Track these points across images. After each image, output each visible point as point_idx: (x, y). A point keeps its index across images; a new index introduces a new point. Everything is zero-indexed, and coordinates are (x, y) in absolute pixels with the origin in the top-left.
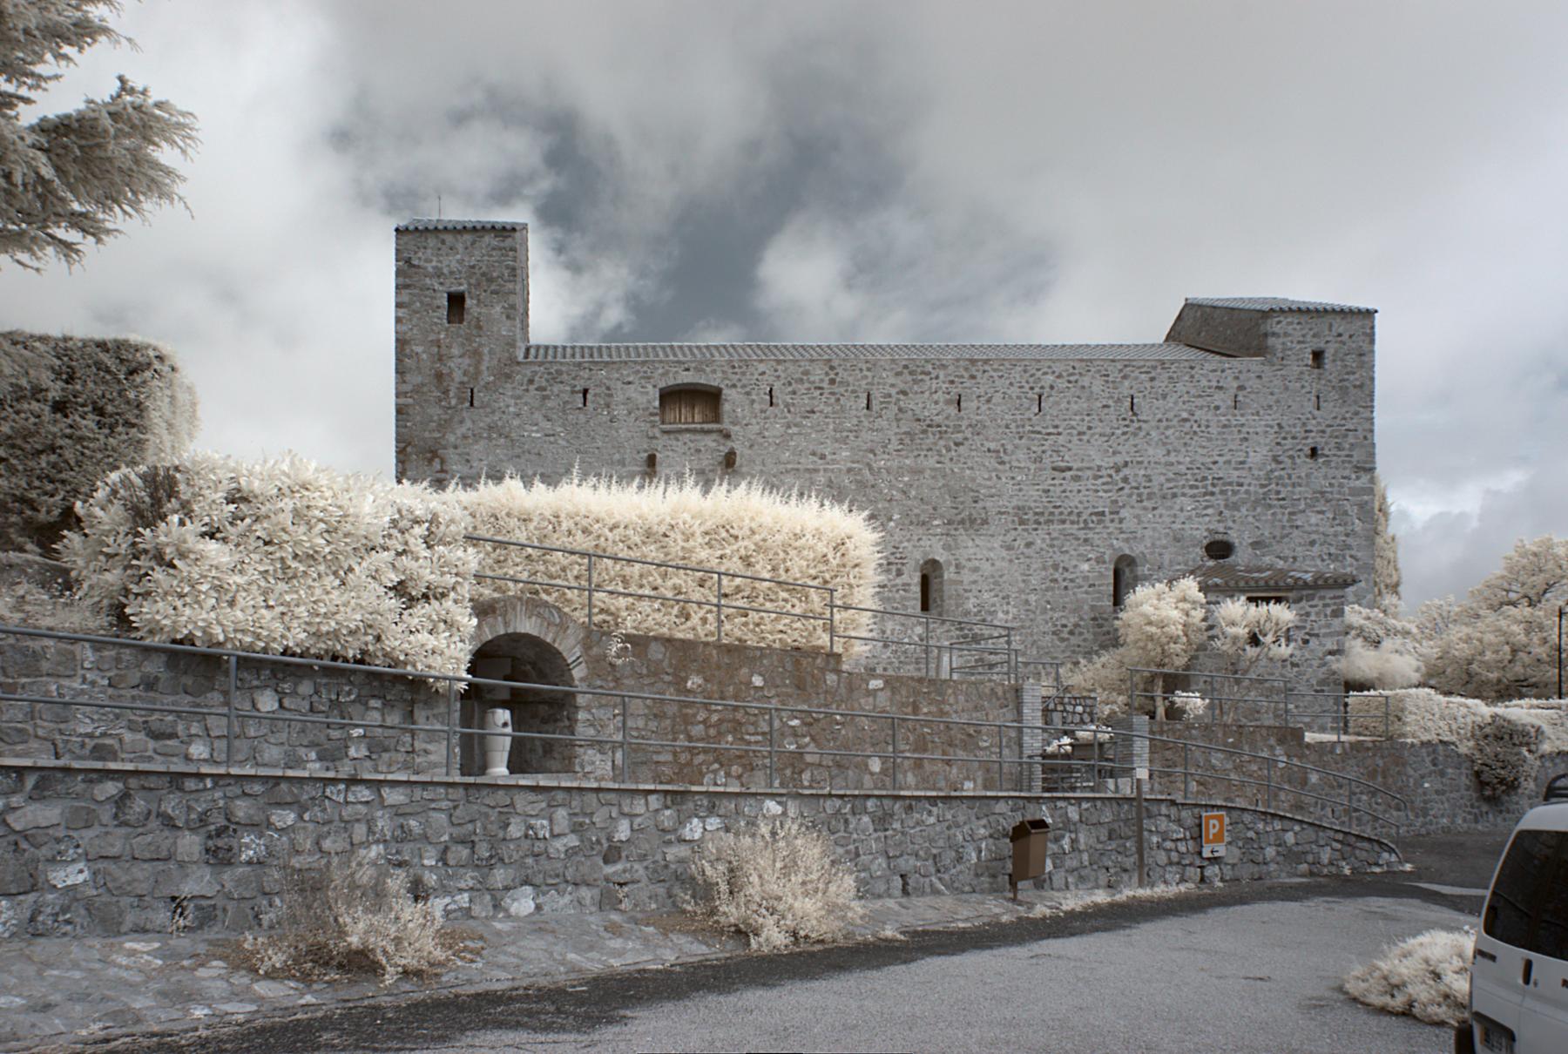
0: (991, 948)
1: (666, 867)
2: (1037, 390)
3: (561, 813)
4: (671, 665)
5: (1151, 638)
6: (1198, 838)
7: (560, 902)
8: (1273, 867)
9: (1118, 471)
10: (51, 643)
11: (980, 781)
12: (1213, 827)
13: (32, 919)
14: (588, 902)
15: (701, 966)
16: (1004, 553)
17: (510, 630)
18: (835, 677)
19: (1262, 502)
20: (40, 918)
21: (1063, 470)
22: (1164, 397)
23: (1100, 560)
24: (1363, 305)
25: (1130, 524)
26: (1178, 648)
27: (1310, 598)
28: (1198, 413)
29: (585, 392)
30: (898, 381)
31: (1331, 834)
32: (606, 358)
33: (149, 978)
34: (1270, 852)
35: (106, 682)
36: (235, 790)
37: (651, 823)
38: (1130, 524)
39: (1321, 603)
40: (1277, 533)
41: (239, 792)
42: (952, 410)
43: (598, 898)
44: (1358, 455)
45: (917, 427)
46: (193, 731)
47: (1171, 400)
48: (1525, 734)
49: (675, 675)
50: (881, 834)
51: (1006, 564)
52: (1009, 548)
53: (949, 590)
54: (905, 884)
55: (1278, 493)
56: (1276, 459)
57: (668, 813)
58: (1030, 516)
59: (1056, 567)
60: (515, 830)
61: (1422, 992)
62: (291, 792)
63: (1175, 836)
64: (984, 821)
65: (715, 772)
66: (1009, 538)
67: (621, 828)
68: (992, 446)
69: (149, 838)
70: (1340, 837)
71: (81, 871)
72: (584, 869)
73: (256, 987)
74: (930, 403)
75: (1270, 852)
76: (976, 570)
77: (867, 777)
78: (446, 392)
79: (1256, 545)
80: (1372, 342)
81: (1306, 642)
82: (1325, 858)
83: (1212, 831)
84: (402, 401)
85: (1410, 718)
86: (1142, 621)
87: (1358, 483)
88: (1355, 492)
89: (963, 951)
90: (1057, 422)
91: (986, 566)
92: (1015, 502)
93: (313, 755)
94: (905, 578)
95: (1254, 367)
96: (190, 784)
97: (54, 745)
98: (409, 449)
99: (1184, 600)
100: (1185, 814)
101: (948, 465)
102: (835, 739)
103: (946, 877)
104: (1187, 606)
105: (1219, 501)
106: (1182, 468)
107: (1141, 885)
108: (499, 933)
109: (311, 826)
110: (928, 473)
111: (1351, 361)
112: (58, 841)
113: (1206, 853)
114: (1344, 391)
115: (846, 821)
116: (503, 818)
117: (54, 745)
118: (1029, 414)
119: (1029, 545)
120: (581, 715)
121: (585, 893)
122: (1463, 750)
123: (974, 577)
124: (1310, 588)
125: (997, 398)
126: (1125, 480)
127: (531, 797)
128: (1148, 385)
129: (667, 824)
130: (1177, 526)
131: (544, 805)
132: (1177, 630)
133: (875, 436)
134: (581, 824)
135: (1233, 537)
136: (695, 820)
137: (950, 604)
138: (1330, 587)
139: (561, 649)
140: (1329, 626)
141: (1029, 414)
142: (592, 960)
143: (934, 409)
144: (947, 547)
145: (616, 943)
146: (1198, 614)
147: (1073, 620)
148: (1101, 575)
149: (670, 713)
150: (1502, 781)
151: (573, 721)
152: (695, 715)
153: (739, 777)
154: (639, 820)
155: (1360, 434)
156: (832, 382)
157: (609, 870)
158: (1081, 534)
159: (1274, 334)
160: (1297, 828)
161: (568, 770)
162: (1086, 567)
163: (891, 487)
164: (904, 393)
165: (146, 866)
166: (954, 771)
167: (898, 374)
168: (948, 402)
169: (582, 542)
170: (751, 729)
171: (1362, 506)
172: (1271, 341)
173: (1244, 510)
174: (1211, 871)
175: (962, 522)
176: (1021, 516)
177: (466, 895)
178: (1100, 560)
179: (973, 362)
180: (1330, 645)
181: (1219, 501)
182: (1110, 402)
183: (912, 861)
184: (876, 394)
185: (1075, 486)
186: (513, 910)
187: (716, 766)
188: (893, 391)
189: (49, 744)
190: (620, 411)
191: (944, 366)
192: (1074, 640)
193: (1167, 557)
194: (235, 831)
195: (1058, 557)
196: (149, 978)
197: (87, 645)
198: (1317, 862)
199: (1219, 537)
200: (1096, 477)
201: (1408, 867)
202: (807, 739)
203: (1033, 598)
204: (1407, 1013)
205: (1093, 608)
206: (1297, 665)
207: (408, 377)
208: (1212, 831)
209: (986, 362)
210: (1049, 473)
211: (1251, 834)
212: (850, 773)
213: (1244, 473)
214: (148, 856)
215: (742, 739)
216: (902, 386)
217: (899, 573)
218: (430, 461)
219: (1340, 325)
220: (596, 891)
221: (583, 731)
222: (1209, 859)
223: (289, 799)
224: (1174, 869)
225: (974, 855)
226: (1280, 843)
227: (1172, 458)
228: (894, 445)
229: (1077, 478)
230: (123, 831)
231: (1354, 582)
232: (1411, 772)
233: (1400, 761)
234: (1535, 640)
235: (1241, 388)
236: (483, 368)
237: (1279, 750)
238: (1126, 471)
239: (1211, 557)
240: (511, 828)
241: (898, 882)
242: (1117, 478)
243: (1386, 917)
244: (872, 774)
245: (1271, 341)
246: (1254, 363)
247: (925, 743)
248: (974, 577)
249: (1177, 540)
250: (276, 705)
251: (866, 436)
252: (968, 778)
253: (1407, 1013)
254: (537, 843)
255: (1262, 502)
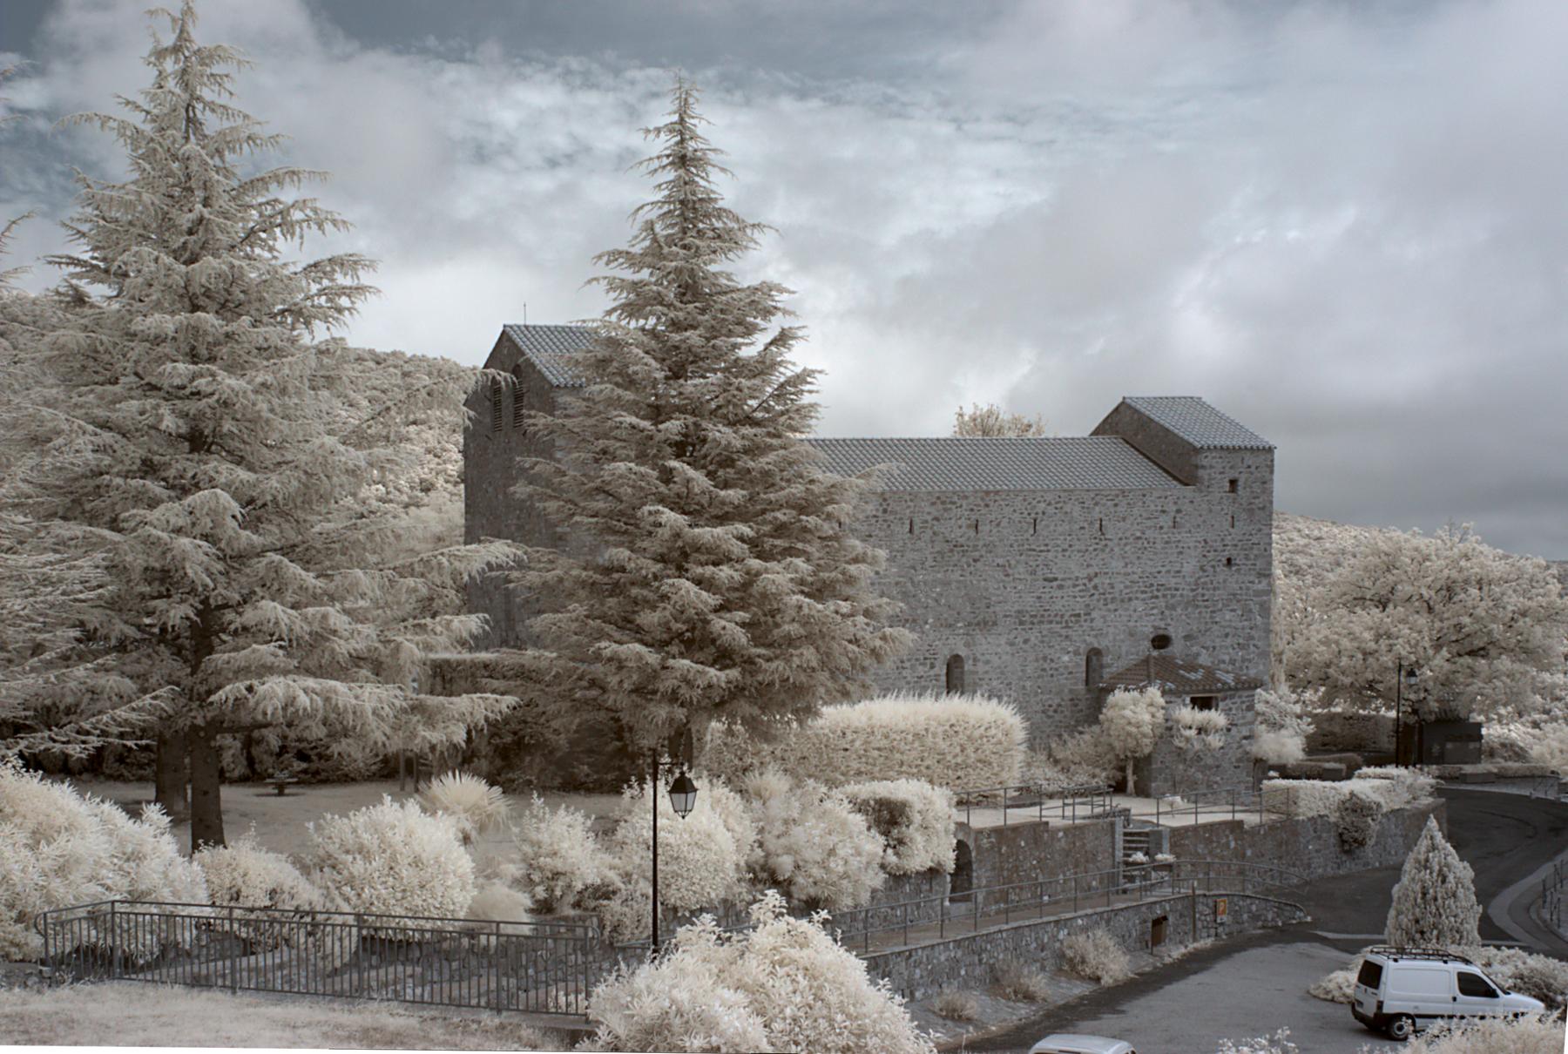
5: (1129, 734)
6: (1215, 913)
9: (1090, 580)
12: (1221, 907)
16: (1008, 648)
19: (1191, 603)
21: (1051, 580)
22: (1124, 519)
23: (1076, 653)
25: (1098, 623)
26: (1147, 741)
27: (1232, 697)
30: (932, 509)
34: (1245, 916)
38: (1098, 623)
40: (1203, 628)
42: (972, 533)
44: (1260, 564)
45: (946, 547)
47: (1128, 521)
48: (1370, 808)
51: (1008, 657)
52: (1012, 644)
56: (1202, 569)
58: (1027, 618)
59: (1045, 659)
61: (1337, 994)
66: (1012, 637)
68: (1000, 561)
74: (956, 529)
75: (1245, 916)
76: (988, 662)
79: (1187, 637)
80: (1272, 472)
85: (1301, 804)
86: (1123, 721)
87: (1260, 587)
88: (1258, 594)
91: (995, 659)
92: (1017, 607)
94: (936, 670)
99: (1151, 705)
101: (969, 578)
104: (1153, 710)
105: (1162, 603)
106: (1136, 577)
107: (1195, 940)
110: (954, 585)
111: (1257, 488)
114: (1251, 512)
118: (1027, 535)
119: (1026, 641)
122: (1332, 819)
123: (987, 668)
125: (1005, 522)
126: (1095, 587)
130: (1131, 624)
132: (1147, 729)
133: (916, 556)
135: (1171, 632)
138: (1244, 689)
141: (1027, 535)
143: (959, 532)
144: (967, 645)
146: (1160, 714)
147: (1057, 701)
148: (1078, 665)
150: (1356, 841)
155: (1262, 547)
156: (885, 511)
158: (1064, 632)
159: (1203, 467)
162: (1066, 658)
163: (927, 596)
164: (936, 519)
167: (933, 504)
168: (969, 526)
169: (884, 743)
171: (1262, 605)
172: (1201, 472)
173: (1179, 610)
174: (1220, 930)
175: (978, 624)
176: (1021, 618)
178: (1076, 653)
179: (987, 493)
180: (1245, 733)
181: (1162, 603)
184: (917, 520)
185: (1059, 593)
188: (929, 518)
191: (966, 497)
192: (1057, 717)
193: (1124, 649)
195: (1047, 651)
199: (1161, 632)
200: (1075, 586)
201: (1309, 919)
203: (1028, 684)
204: (1332, 1000)
205: (1071, 691)
209: (997, 493)
210: (1041, 583)
216: (936, 514)
217: (932, 666)
219: (1250, 459)
226: (1250, 911)
227: (1129, 570)
228: (930, 562)
229: (1060, 587)
233: (1295, 834)
234: (1384, 648)
235: (1179, 511)
238: (1096, 581)
239: (1155, 647)
242: (1090, 586)
243: (1308, 956)
245: (1201, 472)
248: (987, 668)
249: (1131, 635)
251: (909, 555)
253: (1332, 1000)
255: (1191, 603)
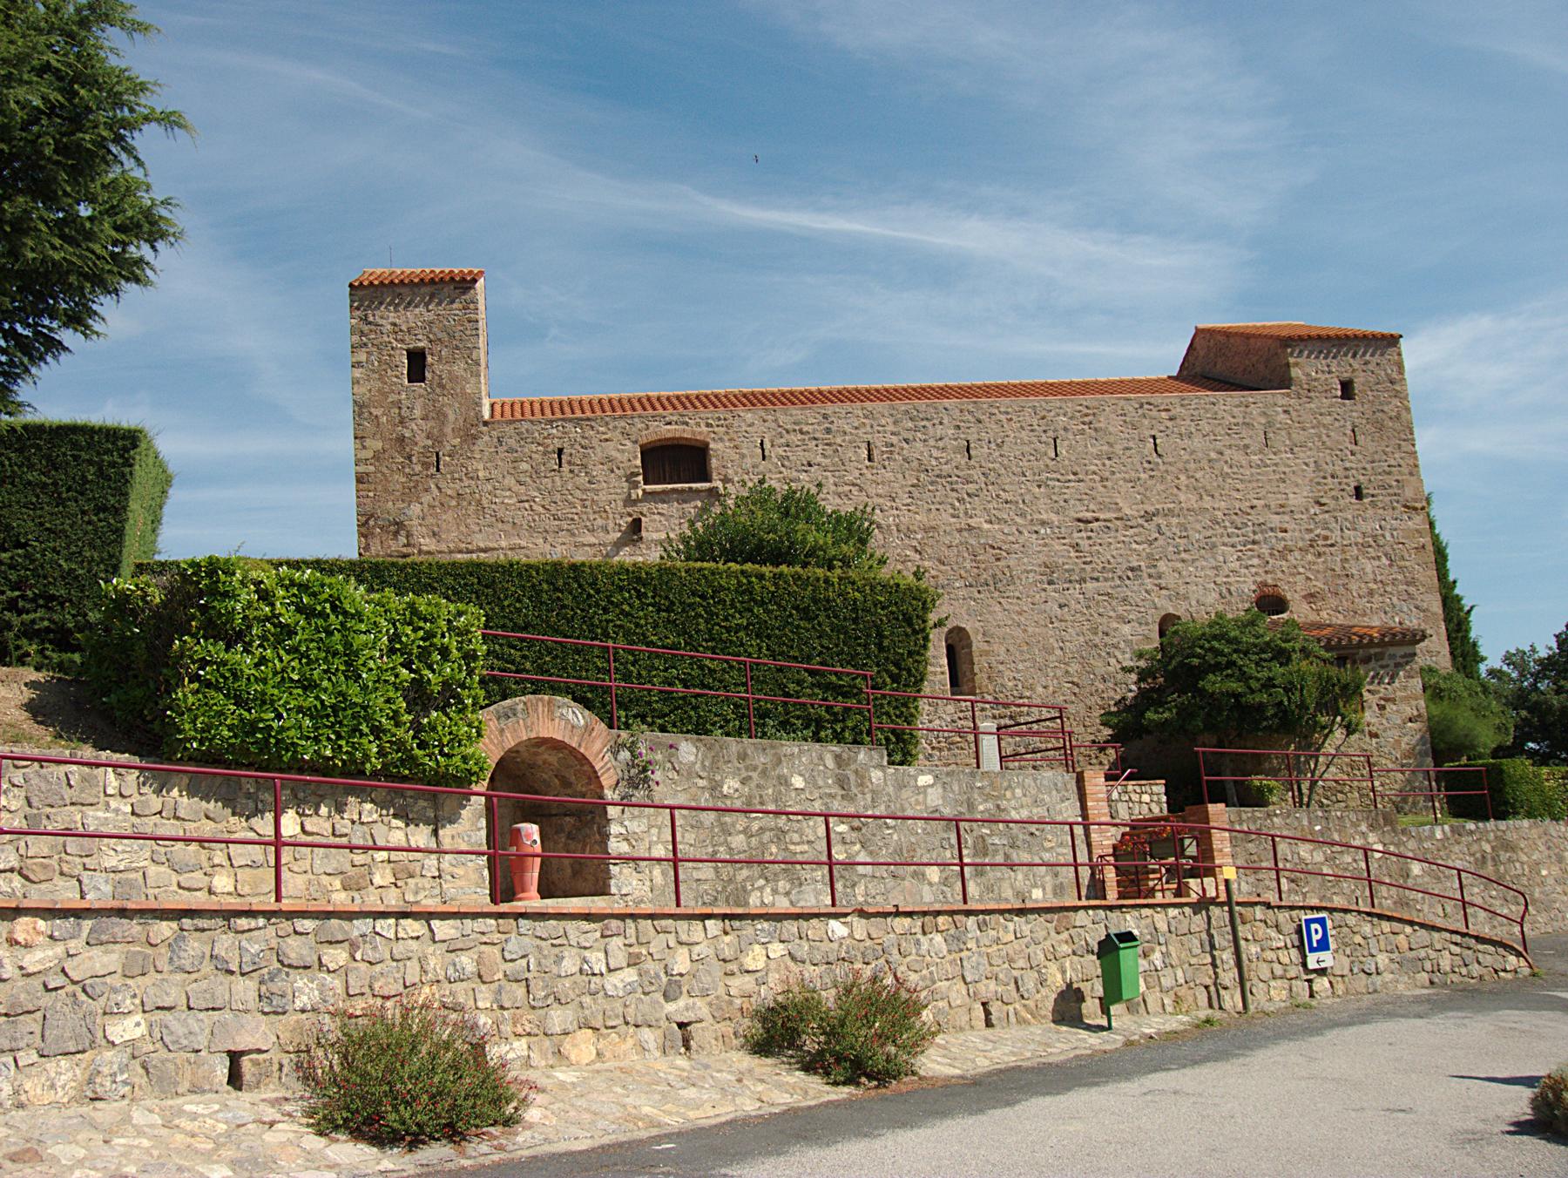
0: (1097, 1084)
1: (731, 1003)
2: (1050, 433)
3: (617, 942)
4: (704, 766)
7: (622, 1046)
8: (1388, 977)
10: (74, 767)
11: (1049, 888)
13: (90, 1082)
14: (652, 1045)
15: (792, 1113)
17: (533, 735)
18: (880, 774)
20: (98, 1080)
24: (1386, 331)
28: (1227, 452)
29: (560, 451)
31: (1447, 935)
32: (579, 414)
33: (218, 1146)
35: (129, 809)
36: (286, 926)
37: (711, 952)
39: (1391, 663)
41: (291, 930)
42: (961, 459)
43: (660, 1041)
46: (216, 861)
49: (711, 780)
50: (957, 956)
53: (980, 663)
54: (988, 1013)
55: (1326, 538)
57: (727, 939)
60: (570, 965)
62: (341, 928)
63: (1274, 945)
64: (1065, 935)
65: (761, 889)
67: (679, 959)
69: (204, 984)
70: (1457, 938)
71: (138, 1024)
72: (645, 1008)
73: (328, 1152)
77: (926, 888)
78: (409, 458)
81: (1382, 708)
82: (1446, 964)
83: (1315, 938)
84: (362, 469)
89: (1069, 1089)
90: (1076, 468)
93: (337, 884)
95: (1282, 401)
96: (243, 923)
97: (80, 882)
98: (371, 523)
100: (1283, 916)
102: (886, 845)
103: (1031, 1003)
108: (562, 1085)
109: (364, 966)
112: (115, 990)
113: (1312, 965)
115: (918, 942)
116: (557, 950)
117: (80, 882)
120: (614, 829)
121: (647, 1034)
124: (1378, 645)
127: (585, 925)
128: (1169, 424)
129: (728, 954)
131: (598, 934)
134: (638, 955)
136: (757, 947)
137: (981, 678)
139: (587, 754)
140: (1405, 688)
142: (670, 1114)
145: (691, 1093)
149: (707, 824)
151: (605, 837)
152: (733, 825)
153: (787, 894)
154: (696, 949)
157: (670, 1007)
160: (1408, 929)
161: (603, 891)
165: (202, 1015)
166: (1020, 877)
168: (956, 450)
170: (796, 838)
174: (1321, 984)
177: (524, 1040)
182: (1131, 444)
183: (992, 985)
184: (878, 442)
186: (573, 1058)
187: (762, 882)
189: (74, 881)
190: (597, 471)
194: (287, 974)
196: (218, 1146)
197: (110, 769)
198: (1438, 969)
202: (858, 847)
206: (1376, 736)
207: (368, 443)
208: (1315, 938)
211: (1358, 939)
212: (906, 883)
213: (1287, 518)
214: (204, 1006)
215: (786, 849)
218: (396, 533)
220: (659, 1032)
221: (616, 846)
222: (1315, 971)
223: (340, 938)
224: (1279, 982)
225: (1059, 976)
230: (179, 977)
231: (1424, 637)
232: (1525, 859)
236: (448, 430)
237: (1372, 838)
240: (565, 963)
241: (979, 1012)
244: (930, 884)
246: (1277, 397)
247: (985, 847)
250: (298, 829)
252: (1035, 886)
254: (594, 979)
